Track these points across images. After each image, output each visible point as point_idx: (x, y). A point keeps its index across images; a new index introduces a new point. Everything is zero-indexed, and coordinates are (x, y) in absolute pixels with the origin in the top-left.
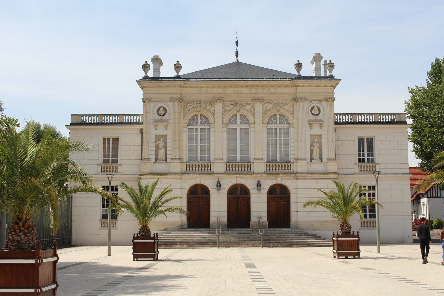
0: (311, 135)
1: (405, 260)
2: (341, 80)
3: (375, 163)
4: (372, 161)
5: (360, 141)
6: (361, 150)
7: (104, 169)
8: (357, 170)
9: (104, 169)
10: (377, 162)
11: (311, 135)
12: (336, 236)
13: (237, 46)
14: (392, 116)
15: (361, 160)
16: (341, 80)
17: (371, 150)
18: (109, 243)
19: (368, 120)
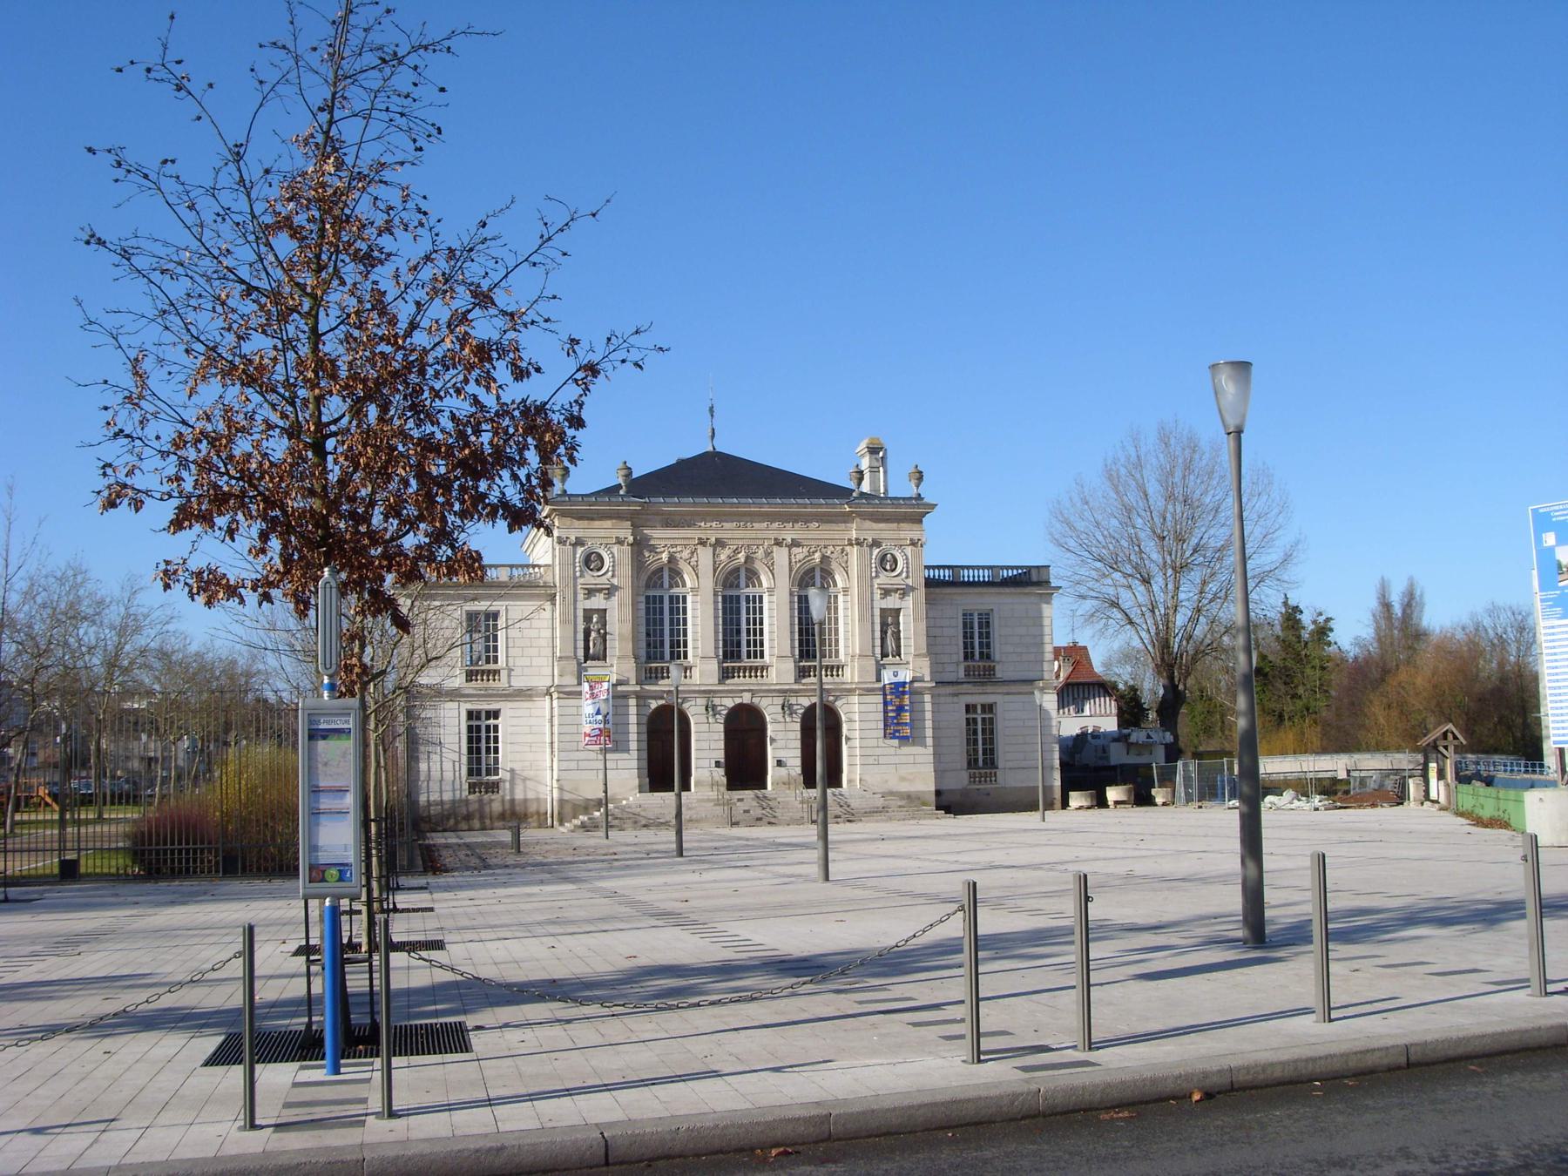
0: (605, 610)
1: (953, 1034)
2: (935, 506)
3: (993, 661)
4: (989, 657)
5: (967, 616)
6: (968, 636)
7: (651, 673)
8: (962, 674)
9: (651, 673)
10: (997, 658)
11: (605, 610)
12: (1070, 744)
13: (712, 416)
14: (1010, 571)
15: (968, 656)
16: (935, 506)
17: (986, 636)
18: (192, 1020)
19: (966, 579)
